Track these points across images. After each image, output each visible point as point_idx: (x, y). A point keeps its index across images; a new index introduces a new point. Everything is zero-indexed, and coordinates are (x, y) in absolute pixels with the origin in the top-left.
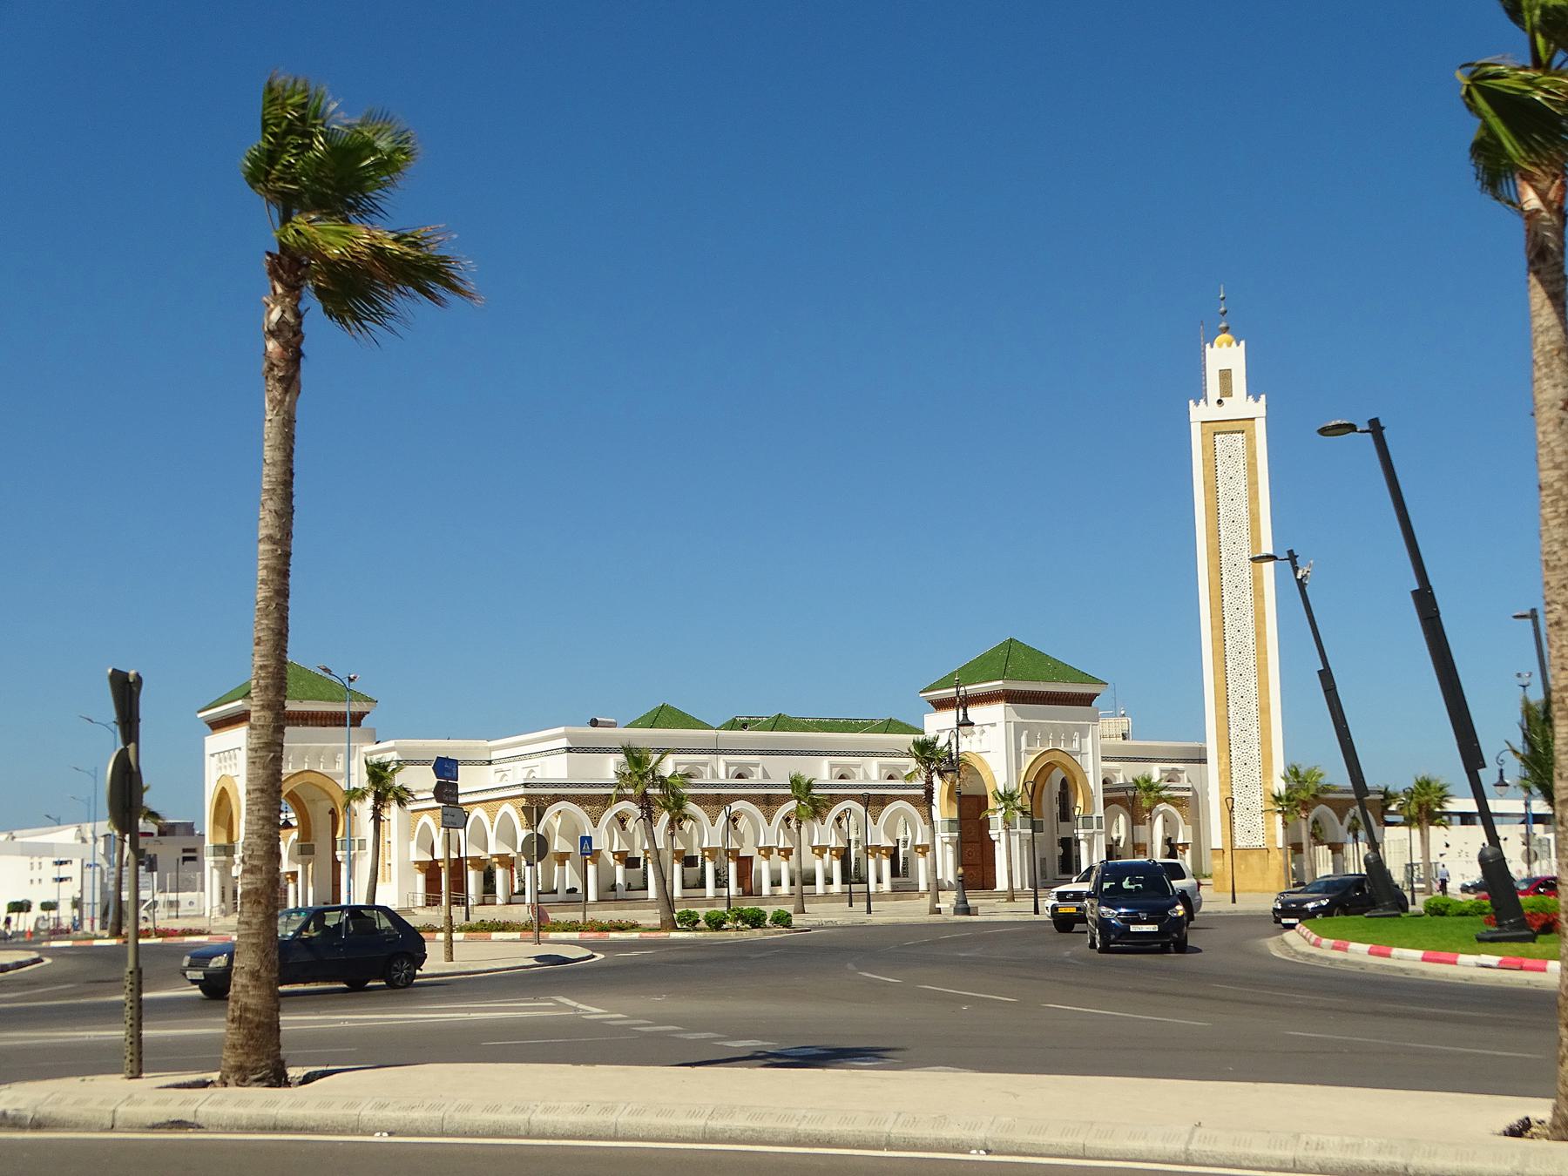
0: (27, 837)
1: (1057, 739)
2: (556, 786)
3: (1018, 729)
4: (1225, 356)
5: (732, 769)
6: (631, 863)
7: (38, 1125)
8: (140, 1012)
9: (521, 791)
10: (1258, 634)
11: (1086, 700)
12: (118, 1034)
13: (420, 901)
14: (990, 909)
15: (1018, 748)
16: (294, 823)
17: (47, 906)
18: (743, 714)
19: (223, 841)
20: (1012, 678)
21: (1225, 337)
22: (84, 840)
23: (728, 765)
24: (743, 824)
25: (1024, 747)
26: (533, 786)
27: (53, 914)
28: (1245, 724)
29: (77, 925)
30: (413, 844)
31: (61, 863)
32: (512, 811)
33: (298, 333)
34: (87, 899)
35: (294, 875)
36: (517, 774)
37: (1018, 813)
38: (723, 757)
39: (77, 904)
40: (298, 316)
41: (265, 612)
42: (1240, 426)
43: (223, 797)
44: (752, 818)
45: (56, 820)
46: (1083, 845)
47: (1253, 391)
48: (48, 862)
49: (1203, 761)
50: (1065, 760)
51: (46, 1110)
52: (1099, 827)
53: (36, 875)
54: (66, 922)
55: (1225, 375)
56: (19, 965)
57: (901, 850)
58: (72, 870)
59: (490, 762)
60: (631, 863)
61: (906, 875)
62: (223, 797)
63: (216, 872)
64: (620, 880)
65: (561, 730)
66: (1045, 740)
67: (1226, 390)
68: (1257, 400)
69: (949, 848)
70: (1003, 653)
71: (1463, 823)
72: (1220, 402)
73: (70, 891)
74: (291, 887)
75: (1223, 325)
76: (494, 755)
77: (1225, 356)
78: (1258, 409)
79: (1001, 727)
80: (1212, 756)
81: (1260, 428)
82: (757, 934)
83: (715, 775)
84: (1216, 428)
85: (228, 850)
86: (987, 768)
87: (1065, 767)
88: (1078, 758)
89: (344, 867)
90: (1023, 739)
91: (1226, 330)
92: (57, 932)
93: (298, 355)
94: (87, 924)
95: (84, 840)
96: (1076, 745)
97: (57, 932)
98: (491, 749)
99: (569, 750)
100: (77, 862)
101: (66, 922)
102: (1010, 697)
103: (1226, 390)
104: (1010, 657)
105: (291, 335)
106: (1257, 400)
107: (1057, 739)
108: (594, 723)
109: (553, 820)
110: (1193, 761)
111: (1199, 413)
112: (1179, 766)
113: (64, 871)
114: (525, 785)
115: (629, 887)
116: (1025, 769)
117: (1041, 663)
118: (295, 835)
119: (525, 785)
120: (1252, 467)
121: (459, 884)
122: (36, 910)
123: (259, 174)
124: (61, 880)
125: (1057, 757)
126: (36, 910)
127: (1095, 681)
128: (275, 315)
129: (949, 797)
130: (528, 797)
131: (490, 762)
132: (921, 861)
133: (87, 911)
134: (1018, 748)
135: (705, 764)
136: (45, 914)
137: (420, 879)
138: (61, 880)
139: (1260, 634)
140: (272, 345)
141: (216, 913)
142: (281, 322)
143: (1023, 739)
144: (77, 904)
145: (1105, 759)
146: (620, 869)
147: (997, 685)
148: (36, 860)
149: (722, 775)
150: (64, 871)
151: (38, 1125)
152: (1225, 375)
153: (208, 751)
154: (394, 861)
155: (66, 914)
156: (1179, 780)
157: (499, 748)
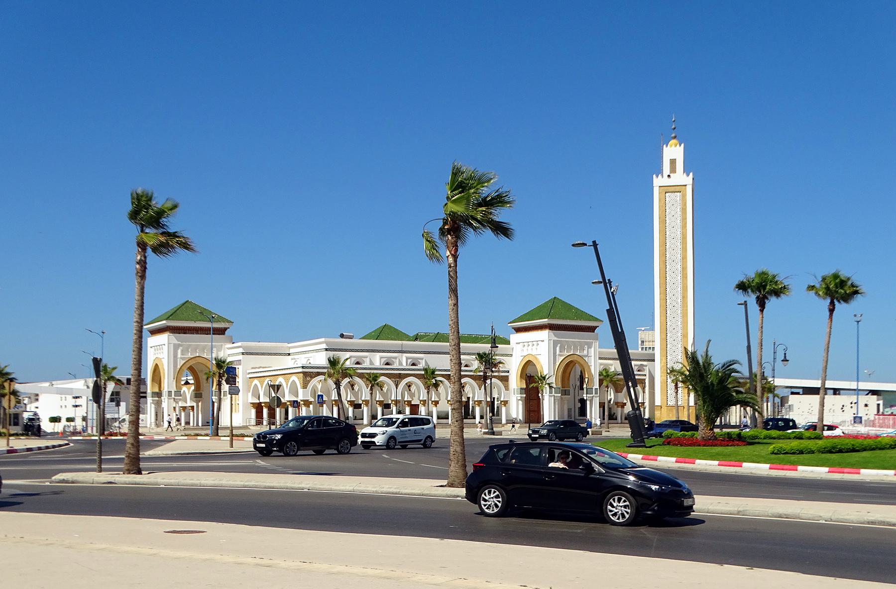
0: (59, 384)
1: (575, 349)
2: (318, 368)
3: (555, 344)
4: (674, 152)
5: (409, 361)
6: (357, 406)
7: (73, 482)
8: (101, 461)
9: (301, 370)
10: (683, 297)
11: (592, 329)
12: (95, 466)
13: (253, 422)
14: (359, 437)
15: (555, 353)
16: (192, 382)
17: (69, 420)
18: (422, 331)
19: (157, 390)
20: (552, 318)
21: (673, 142)
22: (88, 387)
23: (407, 358)
24: (413, 388)
25: (558, 352)
26: (307, 367)
27: (72, 424)
28: (675, 343)
29: (85, 430)
30: (250, 394)
31: (77, 397)
32: (297, 380)
33: (145, 262)
34: (90, 417)
35: (193, 407)
36: (302, 360)
37: (547, 386)
38: (405, 355)
39: (84, 419)
40: (145, 257)
41: (135, 343)
42: (679, 189)
43: (156, 369)
44: (417, 385)
45: (75, 377)
46: (588, 402)
47: (686, 171)
48: (70, 397)
49: (654, 360)
50: (579, 360)
51: (75, 478)
52: (596, 393)
53: (64, 403)
54: (79, 428)
55: (673, 162)
56: (60, 446)
57: (496, 403)
58: (82, 401)
59: (289, 354)
60: (357, 406)
61: (498, 415)
62: (156, 369)
63: (153, 406)
64: (350, 414)
65: (323, 340)
66: (569, 349)
67: (673, 169)
68: (688, 175)
69: (520, 402)
70: (550, 305)
71: (835, 394)
72: (669, 176)
73: (80, 413)
74: (192, 413)
75: (673, 135)
76: (291, 351)
77: (674, 152)
78: (688, 180)
79: (546, 342)
80: (657, 358)
81: (689, 190)
82: (34, 443)
83: (401, 364)
84: (666, 190)
85: (159, 394)
86: (539, 363)
87: (581, 365)
88: (586, 359)
89: (216, 405)
90: (558, 348)
91: (675, 137)
92: (75, 433)
93: (145, 268)
94: (89, 431)
95: (88, 387)
96: (585, 352)
97: (75, 433)
98: (290, 348)
99: (326, 350)
100: (84, 398)
101: (79, 428)
102: (552, 327)
103: (673, 169)
104: (554, 307)
105: (143, 264)
106: (688, 175)
107: (575, 349)
108: (342, 336)
109: (317, 384)
110: (648, 360)
111: (658, 181)
112: (645, 363)
113: (78, 402)
114: (303, 367)
115: (355, 418)
116: (558, 364)
117: (569, 310)
118: (193, 388)
119: (303, 367)
120: (684, 210)
121: (272, 415)
122: (64, 422)
123: (134, 215)
124: (76, 406)
125: (575, 358)
126: (64, 422)
127: (596, 320)
128: (139, 258)
129: (521, 376)
130: (304, 373)
131: (289, 354)
132: (504, 409)
133: (90, 422)
134: (555, 353)
135: (396, 358)
136: (68, 423)
137: (253, 411)
138: (76, 406)
139: (684, 297)
140: (138, 266)
141: (153, 426)
142: (141, 260)
143: (558, 348)
144: (84, 419)
145: (600, 358)
146: (351, 409)
147: (545, 321)
148: (63, 396)
149: (404, 364)
150: (78, 402)
151: (73, 482)
152: (673, 162)
153: (149, 345)
154: (241, 403)
155: (79, 424)
156: (644, 370)
157: (294, 347)
